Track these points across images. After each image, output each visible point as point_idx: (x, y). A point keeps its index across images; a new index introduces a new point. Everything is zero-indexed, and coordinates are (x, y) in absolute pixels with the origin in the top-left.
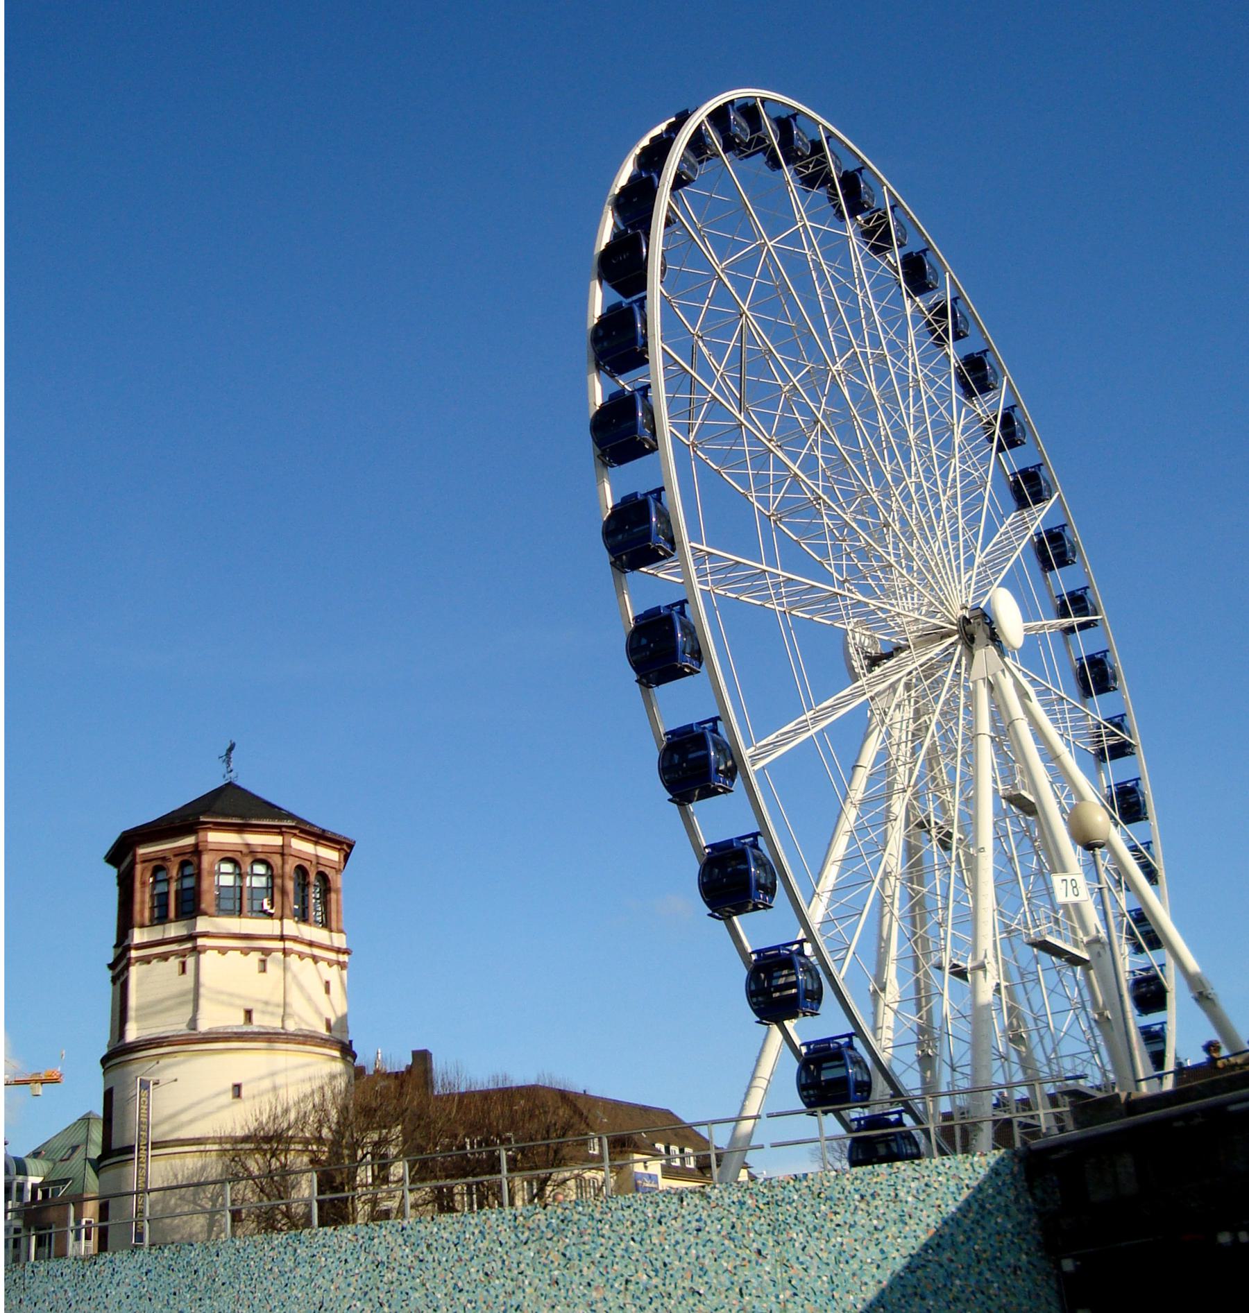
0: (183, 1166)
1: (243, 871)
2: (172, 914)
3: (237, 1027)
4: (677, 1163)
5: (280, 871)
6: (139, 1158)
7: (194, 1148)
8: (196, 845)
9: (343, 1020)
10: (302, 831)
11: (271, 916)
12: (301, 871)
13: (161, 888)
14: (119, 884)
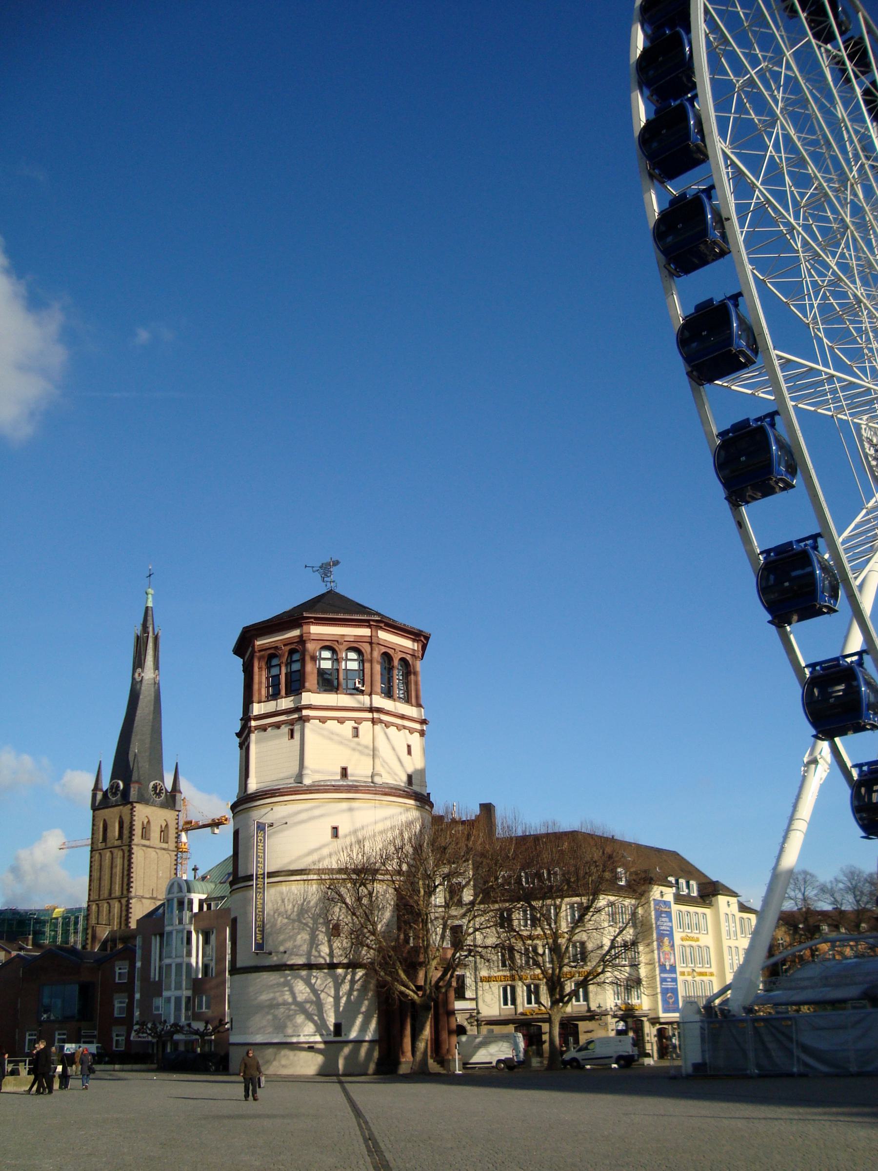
0: (290, 891)
1: (339, 656)
2: (283, 692)
3: (335, 780)
4: (685, 892)
5: (369, 657)
6: (257, 884)
7: (298, 878)
8: (301, 636)
9: (422, 772)
10: (387, 624)
11: (362, 692)
12: (387, 657)
13: (274, 671)
14: (244, 671)
